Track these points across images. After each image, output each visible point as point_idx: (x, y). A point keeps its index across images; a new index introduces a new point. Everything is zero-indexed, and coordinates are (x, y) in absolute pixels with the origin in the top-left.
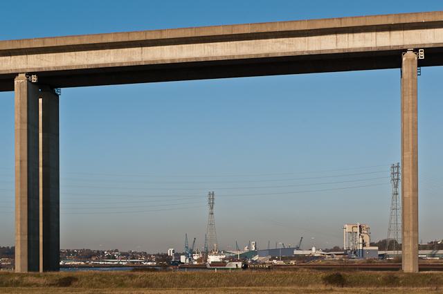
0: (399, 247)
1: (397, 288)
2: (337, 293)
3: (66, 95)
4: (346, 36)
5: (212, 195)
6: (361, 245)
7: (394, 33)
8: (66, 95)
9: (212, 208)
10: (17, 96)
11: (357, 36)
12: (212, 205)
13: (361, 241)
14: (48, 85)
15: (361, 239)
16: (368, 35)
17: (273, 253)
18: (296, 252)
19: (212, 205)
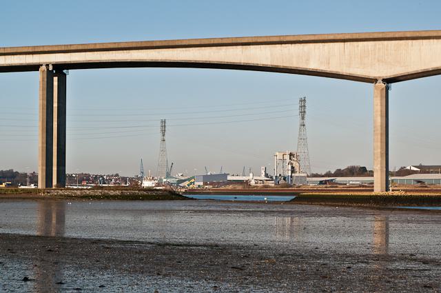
0: (371, 174)
1: (378, 253)
2: (71, 291)
3: (71, 75)
4: (10, 56)
5: (164, 122)
6: (290, 172)
7: (35, 56)
8: (71, 75)
9: (303, 118)
10: (37, 77)
11: (16, 57)
12: (303, 113)
13: (290, 168)
14: (59, 70)
15: (290, 166)
16: (21, 56)
17: (206, 179)
18: (229, 178)
19: (303, 113)
